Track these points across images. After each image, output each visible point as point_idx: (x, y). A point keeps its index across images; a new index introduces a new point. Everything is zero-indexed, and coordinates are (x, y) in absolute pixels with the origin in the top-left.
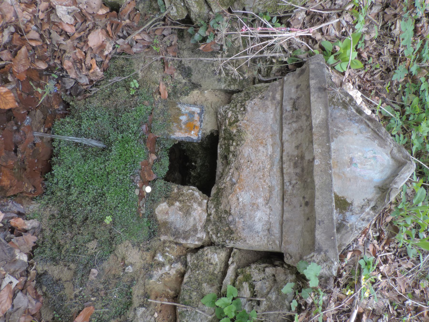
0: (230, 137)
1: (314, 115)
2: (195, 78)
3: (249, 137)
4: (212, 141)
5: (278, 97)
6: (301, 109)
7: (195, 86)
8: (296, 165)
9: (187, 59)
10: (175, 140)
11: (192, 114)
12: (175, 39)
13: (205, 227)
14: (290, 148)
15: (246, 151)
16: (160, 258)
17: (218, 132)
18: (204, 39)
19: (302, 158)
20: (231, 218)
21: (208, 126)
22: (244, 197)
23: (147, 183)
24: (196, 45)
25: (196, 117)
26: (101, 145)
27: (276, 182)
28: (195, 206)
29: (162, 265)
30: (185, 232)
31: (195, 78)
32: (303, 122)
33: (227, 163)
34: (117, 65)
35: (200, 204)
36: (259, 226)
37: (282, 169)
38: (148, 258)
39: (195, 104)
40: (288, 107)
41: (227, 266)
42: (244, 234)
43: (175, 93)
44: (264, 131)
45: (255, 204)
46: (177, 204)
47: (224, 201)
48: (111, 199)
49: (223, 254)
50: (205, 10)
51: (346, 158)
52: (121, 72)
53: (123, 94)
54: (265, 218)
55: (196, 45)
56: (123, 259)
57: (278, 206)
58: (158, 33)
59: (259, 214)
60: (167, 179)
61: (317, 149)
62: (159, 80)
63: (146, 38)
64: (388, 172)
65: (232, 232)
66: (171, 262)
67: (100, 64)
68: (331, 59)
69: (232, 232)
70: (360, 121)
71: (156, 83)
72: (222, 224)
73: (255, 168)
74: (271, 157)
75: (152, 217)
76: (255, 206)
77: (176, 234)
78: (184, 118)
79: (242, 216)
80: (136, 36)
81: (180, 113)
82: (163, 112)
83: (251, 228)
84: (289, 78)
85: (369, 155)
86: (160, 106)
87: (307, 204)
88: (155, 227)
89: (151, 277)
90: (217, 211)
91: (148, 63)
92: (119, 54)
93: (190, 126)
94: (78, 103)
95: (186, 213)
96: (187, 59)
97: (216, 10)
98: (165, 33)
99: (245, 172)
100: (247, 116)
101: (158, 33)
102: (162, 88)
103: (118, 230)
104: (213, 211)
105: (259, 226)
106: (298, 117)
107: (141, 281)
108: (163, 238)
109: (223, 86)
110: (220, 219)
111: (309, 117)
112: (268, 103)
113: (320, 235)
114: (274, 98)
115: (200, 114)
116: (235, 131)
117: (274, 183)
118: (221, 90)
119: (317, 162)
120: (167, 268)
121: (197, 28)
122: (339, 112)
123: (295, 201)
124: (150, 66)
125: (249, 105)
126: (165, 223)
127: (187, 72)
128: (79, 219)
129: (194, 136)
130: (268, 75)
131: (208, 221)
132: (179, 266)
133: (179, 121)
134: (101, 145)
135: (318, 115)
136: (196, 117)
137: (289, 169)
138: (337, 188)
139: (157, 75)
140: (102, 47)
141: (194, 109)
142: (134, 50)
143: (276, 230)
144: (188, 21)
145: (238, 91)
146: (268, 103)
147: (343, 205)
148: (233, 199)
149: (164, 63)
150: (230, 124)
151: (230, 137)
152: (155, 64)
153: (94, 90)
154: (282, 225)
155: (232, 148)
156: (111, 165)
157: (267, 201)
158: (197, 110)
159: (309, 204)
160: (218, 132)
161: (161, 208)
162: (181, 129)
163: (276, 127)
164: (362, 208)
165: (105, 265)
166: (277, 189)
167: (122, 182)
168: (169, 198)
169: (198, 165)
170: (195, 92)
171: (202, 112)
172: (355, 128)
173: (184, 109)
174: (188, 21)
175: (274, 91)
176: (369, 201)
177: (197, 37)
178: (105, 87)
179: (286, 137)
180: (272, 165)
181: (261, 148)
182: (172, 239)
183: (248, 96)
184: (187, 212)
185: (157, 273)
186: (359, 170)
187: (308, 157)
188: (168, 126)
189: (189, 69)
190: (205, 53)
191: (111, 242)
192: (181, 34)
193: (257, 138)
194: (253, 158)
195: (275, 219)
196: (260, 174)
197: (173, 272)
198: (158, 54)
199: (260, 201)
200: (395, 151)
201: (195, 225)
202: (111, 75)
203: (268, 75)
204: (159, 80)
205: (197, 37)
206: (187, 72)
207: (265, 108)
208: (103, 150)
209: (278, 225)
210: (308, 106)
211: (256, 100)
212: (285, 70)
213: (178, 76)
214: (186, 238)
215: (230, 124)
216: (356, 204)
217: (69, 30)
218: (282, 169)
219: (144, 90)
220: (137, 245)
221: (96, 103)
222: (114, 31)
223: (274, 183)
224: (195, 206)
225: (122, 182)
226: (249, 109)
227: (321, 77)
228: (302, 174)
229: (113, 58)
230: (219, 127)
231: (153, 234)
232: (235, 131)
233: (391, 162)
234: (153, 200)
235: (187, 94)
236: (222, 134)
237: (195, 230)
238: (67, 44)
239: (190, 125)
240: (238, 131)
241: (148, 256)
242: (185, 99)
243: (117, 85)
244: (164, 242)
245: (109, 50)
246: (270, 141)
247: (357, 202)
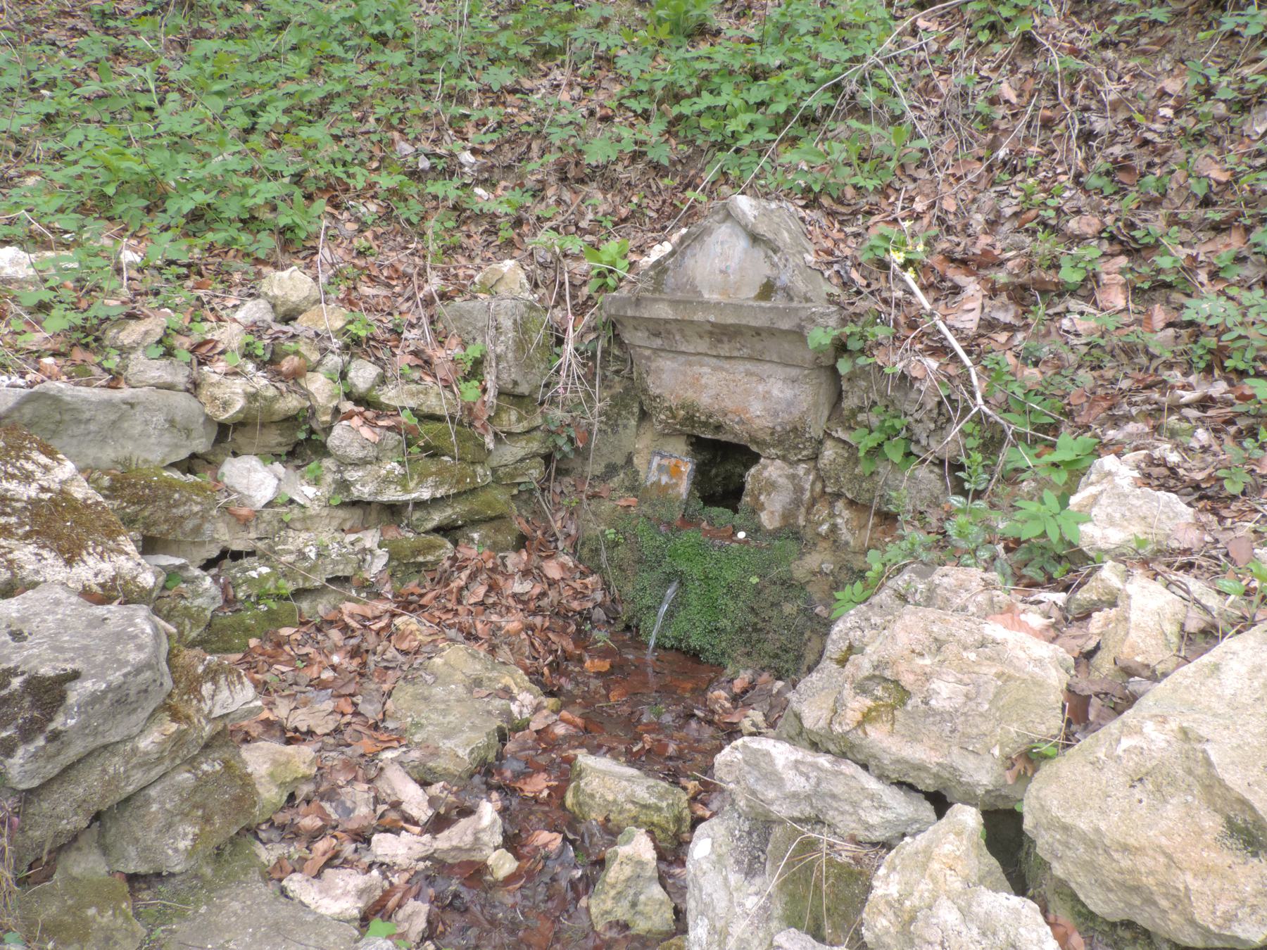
0: (690, 419)
1: (663, 316)
2: (619, 459)
3: (690, 395)
4: (697, 444)
5: (648, 352)
6: (658, 328)
7: (629, 461)
8: (720, 341)
9: (594, 467)
10: (690, 493)
11: (661, 468)
12: (568, 480)
13: (793, 464)
14: (703, 346)
15: (705, 400)
16: (824, 528)
17: (689, 436)
18: (571, 440)
19: (711, 333)
20: (779, 428)
21: (679, 448)
22: (756, 409)
23: (734, 534)
24: (576, 450)
25: (665, 462)
26: (675, 585)
27: (741, 367)
28: (766, 474)
29: (834, 528)
30: (795, 491)
31: (619, 459)
32: (673, 327)
33: (718, 428)
34: (588, 555)
35: (765, 467)
36: (789, 393)
37: (727, 358)
38: (825, 545)
39: (650, 462)
40: (658, 342)
41: (839, 440)
42: (796, 413)
43: (634, 488)
44: (685, 375)
45: (760, 397)
46: (762, 498)
47: (761, 435)
48: (730, 576)
49: (829, 444)
50: (538, 434)
51: (720, 277)
52: (596, 551)
53: (621, 551)
54: (780, 384)
55: (576, 450)
56: (814, 574)
57: (767, 366)
58: (557, 499)
59: (775, 392)
60: (736, 511)
61: (699, 316)
62: (612, 504)
63: (561, 514)
64: (738, 230)
65: (795, 429)
66: (832, 515)
67: (583, 575)
68: (611, 281)
69: (795, 429)
70: (683, 254)
71: (614, 510)
72: (791, 440)
73: (725, 391)
74: (714, 369)
75: (775, 534)
76: (766, 396)
77: (797, 502)
78: (665, 479)
79: (776, 414)
80: (557, 526)
81: (657, 484)
82: (653, 505)
83: (790, 404)
84: (627, 337)
85: (718, 249)
86: (645, 508)
87: (758, 334)
88: (791, 533)
89: (847, 543)
90: (774, 446)
91: (590, 516)
92: (575, 551)
93: (675, 472)
94: (624, 611)
95: (774, 484)
96: (594, 467)
97: (538, 421)
98: (558, 490)
99: (729, 404)
100: (666, 395)
101: (557, 499)
102: (623, 503)
103: (774, 573)
104: (773, 451)
105: (789, 393)
106: (669, 332)
107: (849, 557)
108: (801, 522)
109: (633, 422)
110: (780, 442)
111: (666, 321)
112: (654, 365)
113: (785, 325)
114: (648, 358)
115: (663, 457)
116: (682, 412)
117: (742, 369)
118: (638, 426)
119: (712, 318)
120: (839, 521)
121: (557, 447)
122: (670, 279)
123: (759, 346)
124: (594, 514)
125: (654, 391)
126: (785, 517)
127: (611, 470)
128: (751, 618)
129: (687, 467)
130: (625, 361)
131: (784, 458)
132: (840, 505)
133: (667, 486)
134: (675, 585)
135: (663, 311)
136: (665, 462)
137: (725, 349)
138: (749, 293)
139: (606, 507)
140: (563, 566)
141: (655, 464)
142: (573, 532)
143: (794, 372)
144: (548, 458)
145: (641, 404)
146: (654, 365)
147: (767, 290)
148: (758, 423)
149: (595, 496)
150: (674, 417)
151: (690, 419)
152: (593, 508)
153: (613, 589)
154: (787, 365)
155: (703, 418)
156: (697, 572)
157: (761, 379)
158: (657, 460)
159: (758, 332)
160: (689, 436)
161: (769, 520)
162: (676, 485)
163: (682, 359)
164: (774, 265)
165: (816, 597)
166: (749, 366)
167: (718, 561)
168: (755, 510)
169: (723, 464)
170: (635, 460)
171: (659, 454)
172: (689, 262)
173: (653, 479)
174: (548, 458)
175: (642, 356)
176: (767, 256)
177: (566, 448)
178: (612, 574)
179: (691, 349)
180: (722, 369)
181: (703, 381)
182: (803, 510)
183: (645, 391)
184: (772, 486)
185: (845, 535)
186: (733, 264)
187: (709, 328)
188: (671, 501)
189: (607, 466)
190: (588, 442)
191: (787, 584)
192: (562, 472)
193: (692, 385)
194: (713, 392)
195: (781, 372)
196: (732, 385)
197: (847, 514)
198: (580, 503)
199: (761, 388)
200: (717, 218)
201: (788, 477)
202: (599, 567)
203: (625, 361)
204: (612, 504)
205: (566, 448)
206: (611, 470)
207: (659, 371)
208: (682, 584)
209: (788, 370)
210: (657, 321)
211: (649, 381)
212: (617, 339)
213: (615, 482)
214: (802, 490)
215: (674, 417)
216: (768, 272)
217: (537, 590)
218: (727, 358)
219: (621, 524)
220: (801, 555)
221: (628, 588)
222: (547, 548)
223: (742, 369)
224: (766, 474)
225: (718, 561)
226: (658, 391)
227: (625, 302)
228: (728, 337)
229: (580, 560)
230: (681, 433)
231: (797, 536)
232: (682, 412)
233: (728, 224)
234: (756, 531)
235: (637, 472)
236: (687, 429)
237: (793, 477)
238: (552, 594)
239: (670, 470)
240: (683, 408)
241: (823, 545)
242: (642, 475)
243: (610, 560)
244: (807, 520)
245: (569, 561)
246: (696, 369)
247: (766, 271)
